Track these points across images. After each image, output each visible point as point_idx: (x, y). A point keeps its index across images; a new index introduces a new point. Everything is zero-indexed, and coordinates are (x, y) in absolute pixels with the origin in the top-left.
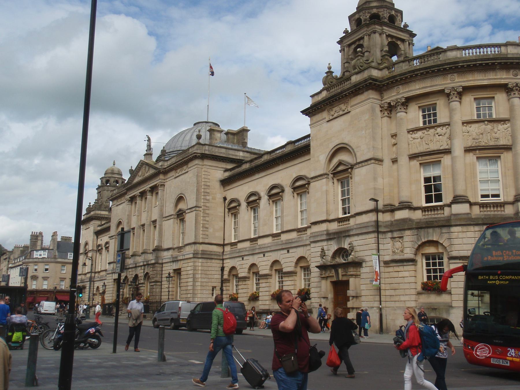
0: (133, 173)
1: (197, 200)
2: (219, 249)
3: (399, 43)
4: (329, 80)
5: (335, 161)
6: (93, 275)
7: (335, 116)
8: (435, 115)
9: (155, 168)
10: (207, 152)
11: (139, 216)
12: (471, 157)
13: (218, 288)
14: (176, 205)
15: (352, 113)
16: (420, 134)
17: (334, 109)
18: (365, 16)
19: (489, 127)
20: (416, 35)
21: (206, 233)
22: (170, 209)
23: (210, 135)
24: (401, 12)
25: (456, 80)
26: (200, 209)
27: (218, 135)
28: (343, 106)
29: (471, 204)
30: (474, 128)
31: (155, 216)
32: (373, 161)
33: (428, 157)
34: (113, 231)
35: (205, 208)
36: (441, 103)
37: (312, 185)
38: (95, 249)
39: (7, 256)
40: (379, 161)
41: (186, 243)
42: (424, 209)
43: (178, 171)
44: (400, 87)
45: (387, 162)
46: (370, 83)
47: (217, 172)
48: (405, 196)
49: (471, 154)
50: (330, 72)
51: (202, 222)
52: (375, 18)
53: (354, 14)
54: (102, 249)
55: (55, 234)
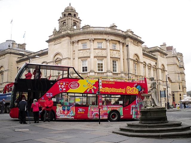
3: (77, 22)
4: (55, 32)
5: (56, 58)
16: (82, 51)
18: (67, 14)
19: (101, 51)
23: (13, 45)
26: (9, 71)
28: (59, 41)
32: (68, 59)
33: (84, 58)
36: (88, 42)
40: (70, 59)
41: (3, 82)
46: (68, 35)
47: (15, 58)
49: (96, 58)
52: (70, 14)
53: (63, 13)
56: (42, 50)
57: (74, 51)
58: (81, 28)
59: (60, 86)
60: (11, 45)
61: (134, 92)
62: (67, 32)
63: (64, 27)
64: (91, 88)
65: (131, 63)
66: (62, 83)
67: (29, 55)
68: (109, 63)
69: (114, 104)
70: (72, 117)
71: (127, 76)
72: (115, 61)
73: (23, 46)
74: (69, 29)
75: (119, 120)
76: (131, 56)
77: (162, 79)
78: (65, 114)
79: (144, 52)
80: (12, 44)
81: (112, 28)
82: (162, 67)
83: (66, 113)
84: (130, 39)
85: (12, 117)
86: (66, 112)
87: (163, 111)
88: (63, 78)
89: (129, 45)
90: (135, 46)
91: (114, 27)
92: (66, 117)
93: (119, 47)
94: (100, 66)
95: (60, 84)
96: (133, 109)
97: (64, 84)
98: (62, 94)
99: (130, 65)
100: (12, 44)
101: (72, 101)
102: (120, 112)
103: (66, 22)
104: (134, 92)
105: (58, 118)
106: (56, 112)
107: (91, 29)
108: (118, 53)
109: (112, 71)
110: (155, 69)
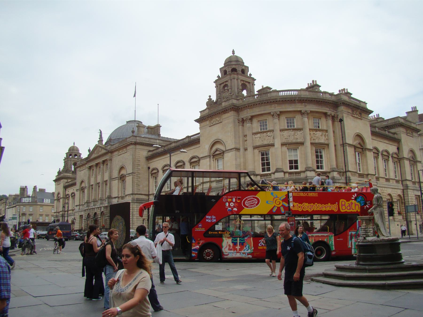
0: (91, 153)
1: (133, 169)
2: (66, 210)
3: (247, 84)
4: (210, 103)
5: (214, 149)
6: (64, 213)
7: (214, 123)
8: (266, 125)
9: (106, 150)
10: (138, 141)
11: (96, 178)
12: (285, 148)
13: (146, 220)
14: (120, 172)
15: (223, 123)
16: (259, 135)
17: (213, 120)
18: (229, 70)
20: (256, 80)
21: (139, 188)
22: (115, 174)
23: (138, 129)
24: (248, 67)
25: (277, 108)
26: (135, 174)
27: (142, 129)
28: (218, 119)
29: (285, 173)
30: (286, 133)
31: (106, 178)
34: (78, 186)
35: (138, 173)
36: (269, 119)
37: (201, 161)
38: (65, 197)
39: (5, 201)
41: (126, 194)
42: (261, 176)
43: (121, 151)
44: (248, 110)
45: (242, 150)
46: (233, 108)
48: (249, 169)
49: (284, 147)
50: (210, 99)
51: (136, 182)
52: (234, 70)
54: (69, 197)
55: (35, 188)
56: (188, 137)
57: (245, 136)
58: (256, 93)
59: (227, 204)
60: (136, 129)
61: (354, 208)
62: (231, 102)
63: (227, 94)
64: (279, 206)
65: (350, 151)
66: (230, 198)
67: (167, 145)
68: (309, 155)
69: (319, 231)
70: (248, 254)
71: (343, 175)
72: (319, 149)
73: (155, 130)
74: (234, 97)
75: (329, 258)
76: (349, 140)
77: (412, 177)
78: (236, 249)
79: (373, 130)
80: (137, 127)
81: (311, 89)
82: (410, 155)
83: (238, 249)
84: (345, 107)
85: (111, 256)
86: (238, 247)
87: (394, 245)
88: (230, 192)
89: (345, 119)
90: (356, 120)
91: (315, 88)
92: (238, 255)
93: (325, 124)
94: (294, 164)
95: (227, 201)
96: (351, 239)
97: (234, 200)
98: (229, 218)
99: (347, 155)
100: (137, 127)
101: (247, 228)
102: (330, 243)
103: (229, 85)
104: (354, 208)
105: (225, 257)
106: (222, 247)
107: (274, 94)
108: (325, 136)
109: (315, 167)
110: (396, 160)
